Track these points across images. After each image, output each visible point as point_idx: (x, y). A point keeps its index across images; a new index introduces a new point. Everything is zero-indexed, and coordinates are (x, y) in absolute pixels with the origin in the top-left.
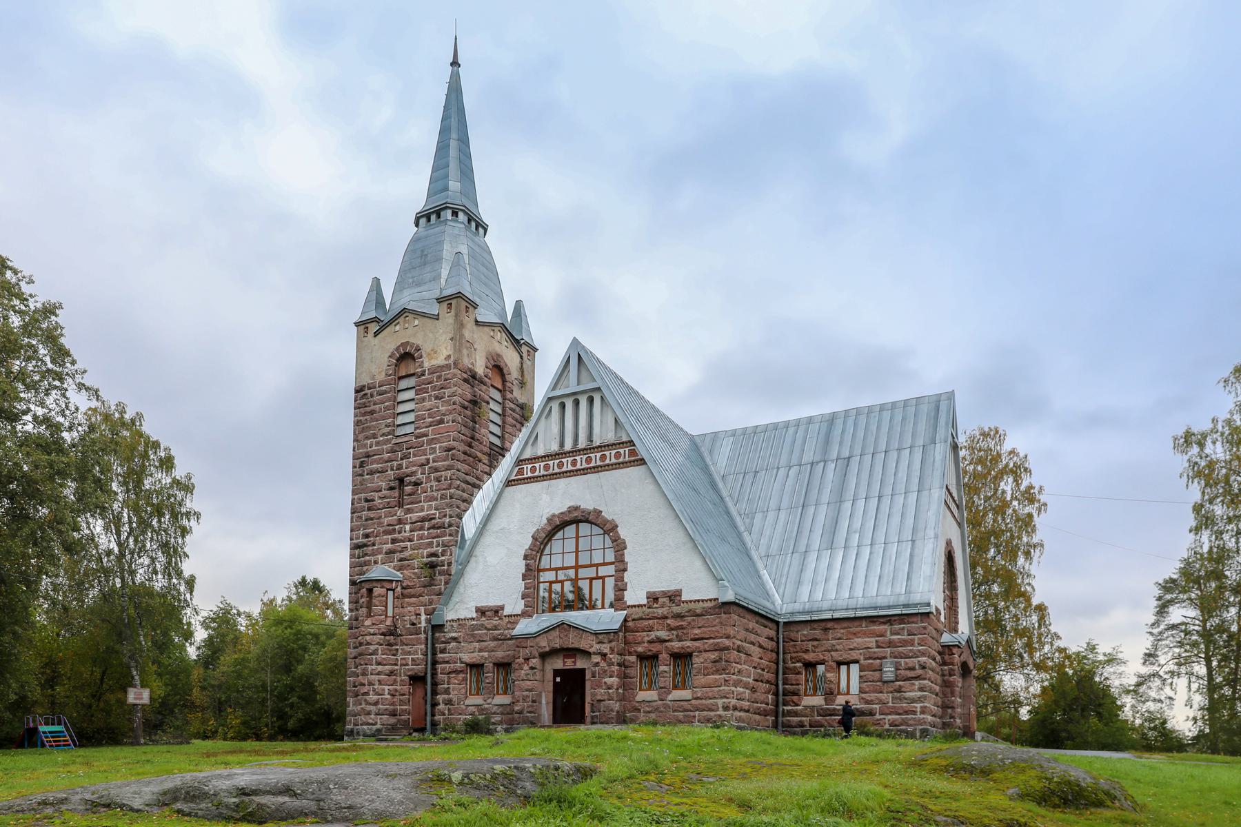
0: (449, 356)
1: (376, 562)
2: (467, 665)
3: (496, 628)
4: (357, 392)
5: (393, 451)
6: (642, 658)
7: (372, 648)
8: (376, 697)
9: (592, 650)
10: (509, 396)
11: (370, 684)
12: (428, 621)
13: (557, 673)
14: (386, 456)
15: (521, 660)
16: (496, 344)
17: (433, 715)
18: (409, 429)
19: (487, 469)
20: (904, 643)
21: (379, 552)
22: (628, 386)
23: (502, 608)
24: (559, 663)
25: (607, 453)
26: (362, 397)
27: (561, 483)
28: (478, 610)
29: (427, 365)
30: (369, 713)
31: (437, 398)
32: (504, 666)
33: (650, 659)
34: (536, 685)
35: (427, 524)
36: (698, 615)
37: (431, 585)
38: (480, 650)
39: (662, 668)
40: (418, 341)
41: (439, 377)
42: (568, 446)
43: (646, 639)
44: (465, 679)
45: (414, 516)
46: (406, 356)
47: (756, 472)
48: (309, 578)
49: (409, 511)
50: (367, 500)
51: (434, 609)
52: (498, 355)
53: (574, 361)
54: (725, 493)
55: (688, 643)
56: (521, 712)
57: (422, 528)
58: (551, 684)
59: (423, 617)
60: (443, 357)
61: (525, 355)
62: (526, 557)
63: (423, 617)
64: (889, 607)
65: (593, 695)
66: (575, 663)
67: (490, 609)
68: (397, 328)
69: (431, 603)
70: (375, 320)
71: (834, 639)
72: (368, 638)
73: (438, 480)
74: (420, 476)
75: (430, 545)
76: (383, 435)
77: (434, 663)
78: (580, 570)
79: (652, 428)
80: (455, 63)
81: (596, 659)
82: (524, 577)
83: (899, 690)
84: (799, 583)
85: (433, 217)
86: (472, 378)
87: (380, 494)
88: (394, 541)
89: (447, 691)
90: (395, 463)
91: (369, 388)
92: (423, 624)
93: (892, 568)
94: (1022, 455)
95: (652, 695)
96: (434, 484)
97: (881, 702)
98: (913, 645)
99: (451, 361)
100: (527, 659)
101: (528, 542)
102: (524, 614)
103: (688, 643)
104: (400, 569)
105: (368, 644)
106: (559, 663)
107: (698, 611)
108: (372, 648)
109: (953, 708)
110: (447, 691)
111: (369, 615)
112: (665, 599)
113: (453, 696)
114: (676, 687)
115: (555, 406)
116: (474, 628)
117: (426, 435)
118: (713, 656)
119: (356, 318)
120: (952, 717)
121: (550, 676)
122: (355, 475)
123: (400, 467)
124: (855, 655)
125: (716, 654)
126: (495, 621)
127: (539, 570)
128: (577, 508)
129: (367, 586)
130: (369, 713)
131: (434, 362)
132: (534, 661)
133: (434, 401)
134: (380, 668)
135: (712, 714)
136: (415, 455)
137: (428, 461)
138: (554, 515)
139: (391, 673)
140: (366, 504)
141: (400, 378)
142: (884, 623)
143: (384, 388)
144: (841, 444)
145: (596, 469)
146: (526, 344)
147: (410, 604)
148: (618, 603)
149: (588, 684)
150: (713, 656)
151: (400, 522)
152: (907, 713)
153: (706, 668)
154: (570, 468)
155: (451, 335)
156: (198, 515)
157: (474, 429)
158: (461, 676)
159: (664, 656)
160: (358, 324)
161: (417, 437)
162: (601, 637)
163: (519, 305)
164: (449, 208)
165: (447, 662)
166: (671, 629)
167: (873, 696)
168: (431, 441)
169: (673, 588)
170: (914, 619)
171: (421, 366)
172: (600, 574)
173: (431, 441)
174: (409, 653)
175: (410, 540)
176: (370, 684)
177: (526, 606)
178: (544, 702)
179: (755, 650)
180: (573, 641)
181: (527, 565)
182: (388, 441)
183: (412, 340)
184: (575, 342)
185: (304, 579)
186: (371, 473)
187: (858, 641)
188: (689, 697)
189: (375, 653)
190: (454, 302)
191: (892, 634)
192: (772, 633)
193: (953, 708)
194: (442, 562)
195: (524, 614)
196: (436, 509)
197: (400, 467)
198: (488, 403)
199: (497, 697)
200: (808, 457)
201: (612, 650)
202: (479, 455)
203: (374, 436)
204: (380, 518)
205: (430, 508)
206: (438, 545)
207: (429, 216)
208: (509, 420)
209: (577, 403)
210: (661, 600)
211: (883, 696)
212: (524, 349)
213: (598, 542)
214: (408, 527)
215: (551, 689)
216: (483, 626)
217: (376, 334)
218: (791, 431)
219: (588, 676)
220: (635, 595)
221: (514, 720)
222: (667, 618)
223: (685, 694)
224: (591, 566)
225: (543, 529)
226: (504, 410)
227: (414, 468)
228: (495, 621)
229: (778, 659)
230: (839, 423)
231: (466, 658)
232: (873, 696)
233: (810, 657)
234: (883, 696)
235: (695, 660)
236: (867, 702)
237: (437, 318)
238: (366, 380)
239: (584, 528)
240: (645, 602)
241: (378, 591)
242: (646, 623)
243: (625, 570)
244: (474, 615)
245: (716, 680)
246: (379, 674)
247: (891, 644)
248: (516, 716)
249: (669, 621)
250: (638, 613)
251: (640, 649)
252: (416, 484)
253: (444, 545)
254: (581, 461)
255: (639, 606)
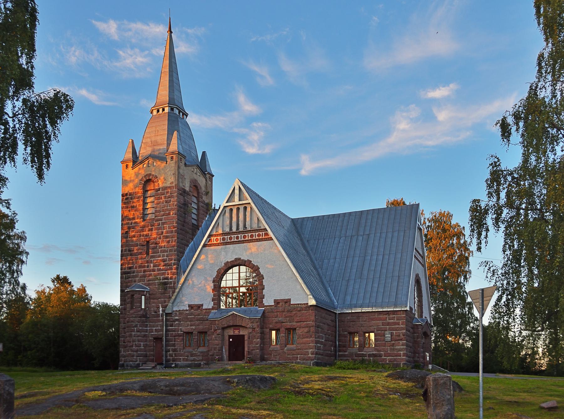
0: (172, 183)
1: (135, 281)
2: (184, 332)
4: (123, 195)
9: (248, 326)
10: (201, 200)
12: (163, 311)
13: (230, 337)
16: (195, 175)
19: (191, 236)
21: (136, 276)
22: (262, 199)
23: (202, 305)
24: (231, 332)
27: (231, 246)
28: (189, 306)
30: (133, 356)
32: (203, 333)
37: (164, 293)
42: (234, 229)
44: (183, 339)
46: (148, 181)
47: (324, 239)
48: (62, 276)
50: (130, 251)
52: (196, 180)
53: (237, 192)
54: (309, 249)
58: (228, 342)
61: (208, 179)
63: (161, 309)
65: (249, 347)
66: (239, 332)
73: (168, 242)
78: (241, 288)
79: (274, 220)
83: (393, 345)
84: (346, 295)
86: (183, 192)
89: (174, 345)
92: (161, 312)
94: (462, 227)
98: (399, 325)
101: (215, 274)
103: (294, 323)
104: (148, 285)
106: (231, 332)
108: (134, 324)
109: (419, 353)
111: (132, 308)
116: (187, 315)
120: (418, 358)
122: (122, 237)
124: (372, 329)
128: (239, 259)
129: (131, 293)
130: (133, 356)
132: (219, 331)
135: (306, 356)
138: (228, 262)
142: (386, 314)
146: (209, 173)
149: (246, 343)
152: (396, 356)
154: (235, 240)
156: (27, 253)
157: (185, 218)
160: (122, 162)
163: (204, 153)
165: (174, 331)
168: (163, 224)
170: (399, 313)
177: (214, 304)
179: (326, 327)
185: (58, 276)
192: (333, 318)
193: (419, 353)
194: (171, 282)
198: (191, 204)
200: (349, 233)
202: (188, 230)
205: (163, 256)
208: (201, 212)
209: (238, 209)
210: (281, 304)
212: (208, 176)
218: (341, 219)
219: (246, 338)
221: (209, 360)
226: (198, 207)
228: (199, 312)
229: (336, 330)
230: (364, 216)
231: (184, 329)
233: (351, 330)
240: (273, 304)
241: (136, 296)
244: (188, 309)
247: (388, 324)
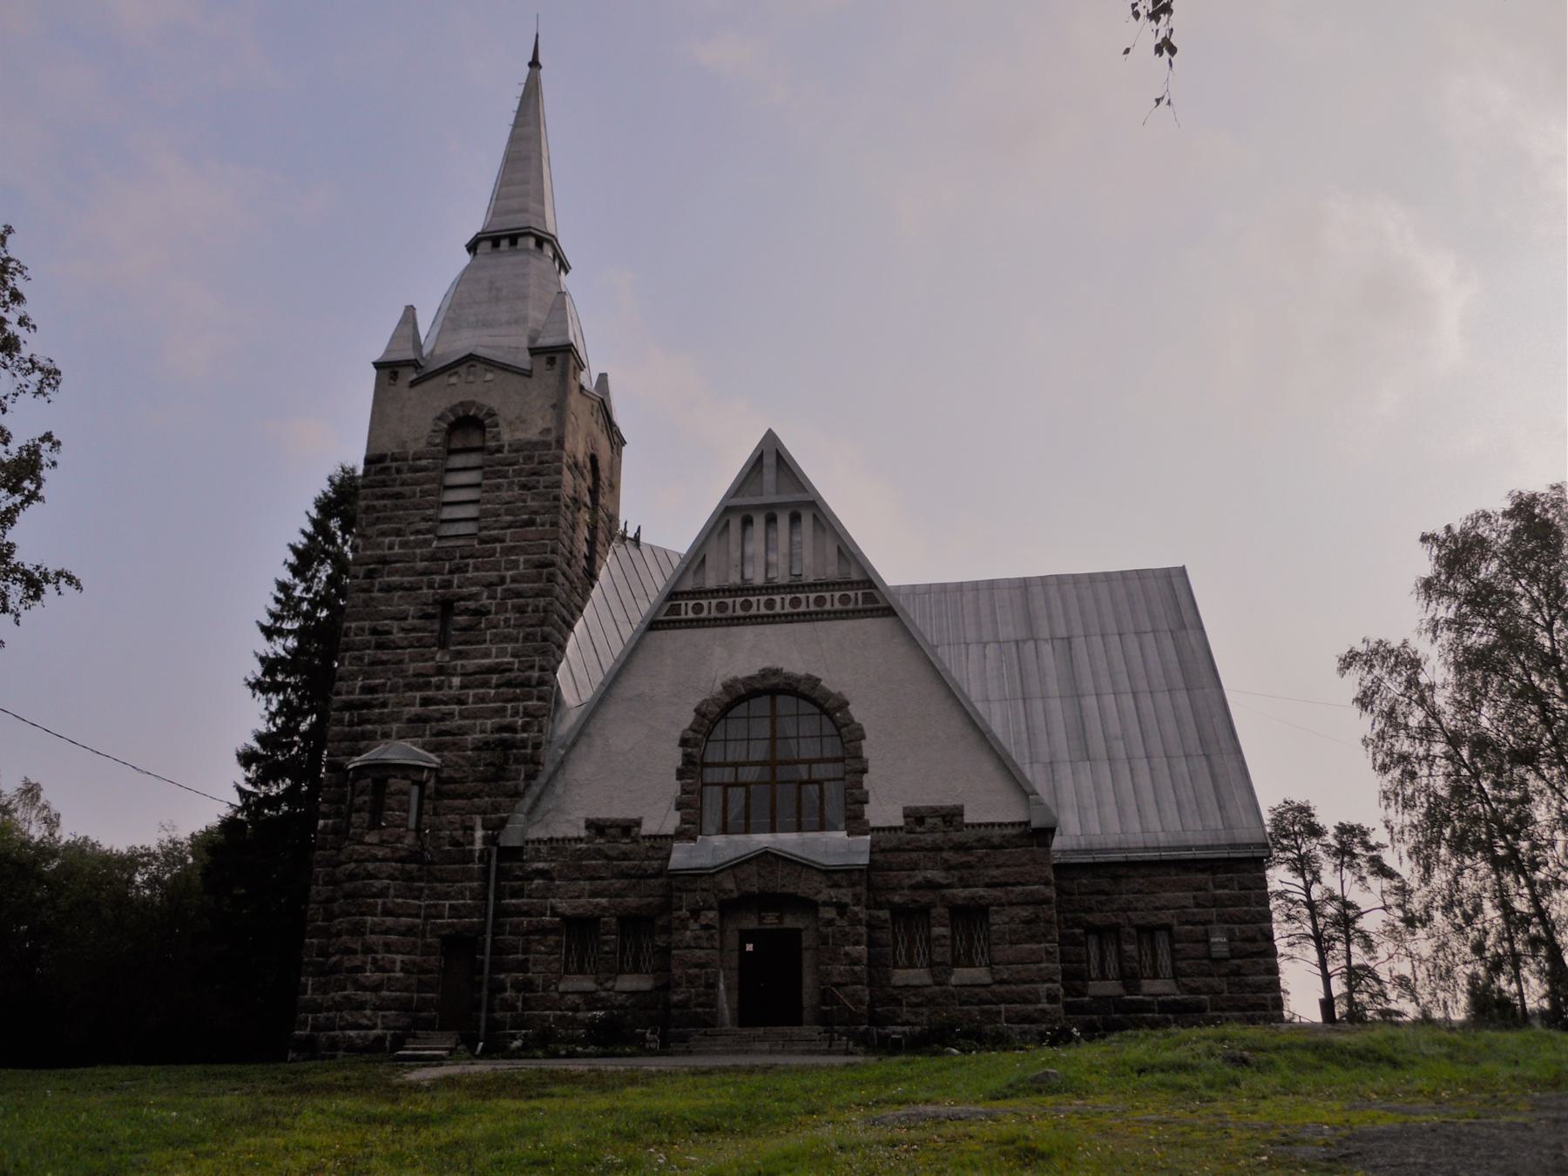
0: (547, 431)
1: (386, 735)
3: (625, 856)
5: (433, 558)
6: (898, 912)
7: (378, 884)
8: (377, 976)
11: (368, 950)
14: (421, 565)
15: (684, 913)
17: (491, 1010)
18: (463, 529)
20: (1236, 901)
21: (395, 717)
23: (638, 823)
25: (705, 603)
26: (378, 472)
27: (748, 633)
28: (591, 824)
29: (506, 437)
30: (361, 1006)
31: (524, 487)
32: (635, 924)
33: (911, 916)
34: (710, 959)
35: (495, 678)
36: (994, 847)
38: (594, 894)
39: (937, 931)
40: (492, 401)
41: (531, 458)
43: (907, 882)
44: (558, 944)
45: (472, 664)
49: (460, 655)
50: (374, 631)
51: (504, 821)
53: (770, 461)
55: (981, 891)
56: (683, 1005)
57: (485, 684)
58: (736, 955)
59: (479, 834)
60: (537, 431)
62: (684, 742)
64: (1208, 847)
66: (781, 919)
67: (615, 824)
68: (454, 380)
69: (496, 809)
70: (414, 364)
71: (1128, 892)
72: (370, 866)
73: (521, 610)
74: (485, 600)
75: (500, 712)
76: (418, 532)
77: (501, 912)
80: (535, 64)
81: (830, 913)
82: (681, 774)
83: (1237, 972)
85: (504, 244)
87: (404, 624)
88: (426, 702)
89: (522, 966)
90: (437, 578)
91: (394, 459)
92: (478, 845)
93: (1190, 792)
95: (918, 976)
96: (511, 615)
97: (1212, 990)
99: (551, 438)
100: (695, 913)
101: (687, 718)
102: (680, 835)
103: (981, 891)
104: (435, 749)
105: (370, 876)
107: (996, 841)
108: (378, 884)
110: (522, 966)
111: (374, 825)
112: (935, 824)
113: (536, 975)
114: (957, 963)
115: (735, 524)
117: (501, 540)
118: (1025, 913)
119: (378, 355)
121: (733, 941)
123: (447, 584)
125: (1030, 909)
126: (625, 845)
127: (705, 765)
128: (776, 672)
130: (361, 1006)
131: (520, 435)
132: (711, 914)
133: (517, 492)
134: (389, 921)
135: (1030, 1008)
136: (476, 569)
137: (502, 580)
138: (736, 680)
139: (410, 930)
140: (373, 639)
141: (452, 452)
142: (1203, 871)
143: (424, 462)
144: (1050, 618)
145: (788, 618)
147: (453, 810)
148: (855, 823)
150: (1025, 913)
151: (440, 670)
153: (1015, 932)
154: (763, 611)
155: (554, 401)
158: (552, 939)
159: (940, 911)
161: (482, 541)
162: (836, 877)
163: (603, 377)
164: (514, 238)
165: (527, 914)
166: (949, 868)
167: (1198, 982)
168: (508, 551)
169: (949, 802)
171: (497, 437)
172: (742, 779)
173: (508, 551)
174: (447, 896)
175: (461, 702)
176: (368, 950)
177: (683, 821)
178: (722, 987)
180: (784, 883)
181: (685, 755)
182: (427, 543)
183: (480, 400)
184: (770, 437)
186: (388, 588)
187: (1168, 896)
188: (987, 980)
189: (383, 893)
190: (559, 357)
191: (1216, 887)
194: (523, 741)
195: (680, 835)
196: (514, 655)
197: (447, 584)
199: (621, 978)
201: (857, 899)
203: (398, 533)
204: (401, 661)
205: (502, 653)
206: (515, 713)
207: (487, 242)
210: (929, 821)
211: (1215, 981)
213: (810, 725)
214: (456, 681)
215: (735, 963)
216: (598, 853)
217: (413, 384)
219: (807, 940)
220: (884, 811)
222: (941, 849)
223: (979, 974)
224: (725, 765)
225: (714, 700)
227: (474, 589)
228: (625, 845)
232: (1198, 982)
234: (1215, 981)
235: (994, 918)
236: (1193, 991)
237: (528, 374)
238: (390, 448)
239: (785, 704)
240: (900, 822)
241: (395, 784)
242: (906, 856)
243: (865, 771)
244: (583, 833)
245: (1033, 952)
246: (388, 931)
247: (1216, 902)
248: (674, 1012)
249: (945, 855)
250: (893, 840)
251: (897, 899)
252: (480, 613)
253: (526, 714)
254: (782, 603)
255: (890, 829)
